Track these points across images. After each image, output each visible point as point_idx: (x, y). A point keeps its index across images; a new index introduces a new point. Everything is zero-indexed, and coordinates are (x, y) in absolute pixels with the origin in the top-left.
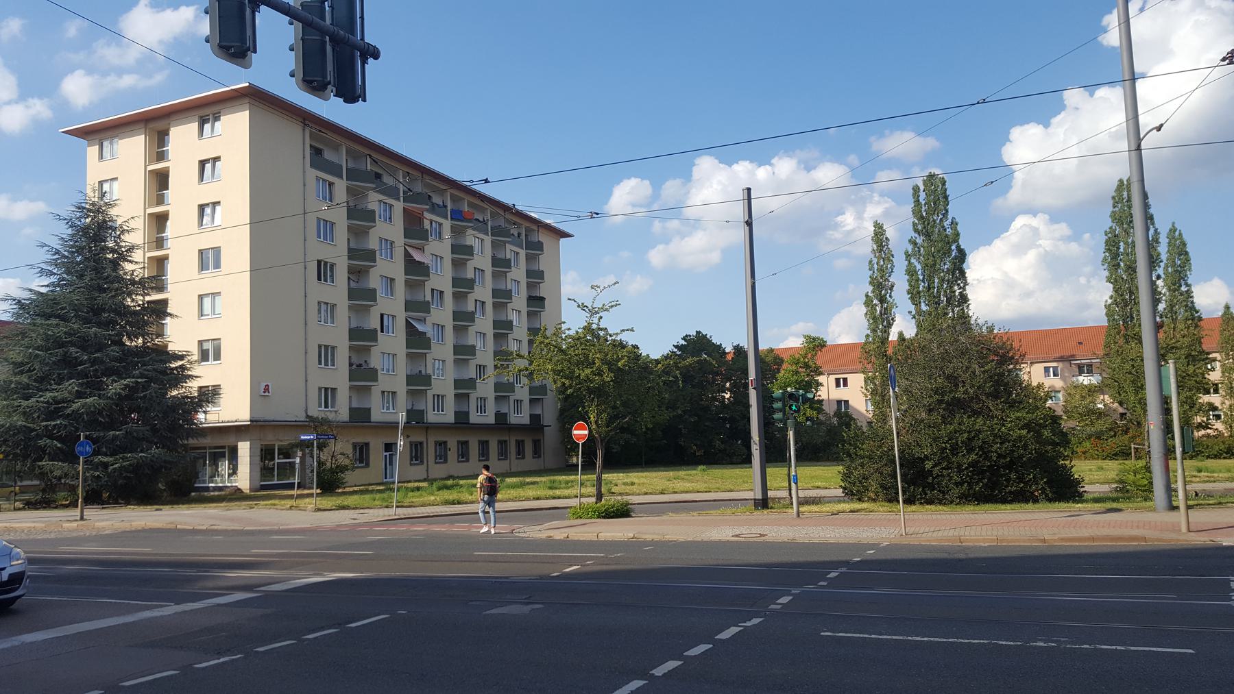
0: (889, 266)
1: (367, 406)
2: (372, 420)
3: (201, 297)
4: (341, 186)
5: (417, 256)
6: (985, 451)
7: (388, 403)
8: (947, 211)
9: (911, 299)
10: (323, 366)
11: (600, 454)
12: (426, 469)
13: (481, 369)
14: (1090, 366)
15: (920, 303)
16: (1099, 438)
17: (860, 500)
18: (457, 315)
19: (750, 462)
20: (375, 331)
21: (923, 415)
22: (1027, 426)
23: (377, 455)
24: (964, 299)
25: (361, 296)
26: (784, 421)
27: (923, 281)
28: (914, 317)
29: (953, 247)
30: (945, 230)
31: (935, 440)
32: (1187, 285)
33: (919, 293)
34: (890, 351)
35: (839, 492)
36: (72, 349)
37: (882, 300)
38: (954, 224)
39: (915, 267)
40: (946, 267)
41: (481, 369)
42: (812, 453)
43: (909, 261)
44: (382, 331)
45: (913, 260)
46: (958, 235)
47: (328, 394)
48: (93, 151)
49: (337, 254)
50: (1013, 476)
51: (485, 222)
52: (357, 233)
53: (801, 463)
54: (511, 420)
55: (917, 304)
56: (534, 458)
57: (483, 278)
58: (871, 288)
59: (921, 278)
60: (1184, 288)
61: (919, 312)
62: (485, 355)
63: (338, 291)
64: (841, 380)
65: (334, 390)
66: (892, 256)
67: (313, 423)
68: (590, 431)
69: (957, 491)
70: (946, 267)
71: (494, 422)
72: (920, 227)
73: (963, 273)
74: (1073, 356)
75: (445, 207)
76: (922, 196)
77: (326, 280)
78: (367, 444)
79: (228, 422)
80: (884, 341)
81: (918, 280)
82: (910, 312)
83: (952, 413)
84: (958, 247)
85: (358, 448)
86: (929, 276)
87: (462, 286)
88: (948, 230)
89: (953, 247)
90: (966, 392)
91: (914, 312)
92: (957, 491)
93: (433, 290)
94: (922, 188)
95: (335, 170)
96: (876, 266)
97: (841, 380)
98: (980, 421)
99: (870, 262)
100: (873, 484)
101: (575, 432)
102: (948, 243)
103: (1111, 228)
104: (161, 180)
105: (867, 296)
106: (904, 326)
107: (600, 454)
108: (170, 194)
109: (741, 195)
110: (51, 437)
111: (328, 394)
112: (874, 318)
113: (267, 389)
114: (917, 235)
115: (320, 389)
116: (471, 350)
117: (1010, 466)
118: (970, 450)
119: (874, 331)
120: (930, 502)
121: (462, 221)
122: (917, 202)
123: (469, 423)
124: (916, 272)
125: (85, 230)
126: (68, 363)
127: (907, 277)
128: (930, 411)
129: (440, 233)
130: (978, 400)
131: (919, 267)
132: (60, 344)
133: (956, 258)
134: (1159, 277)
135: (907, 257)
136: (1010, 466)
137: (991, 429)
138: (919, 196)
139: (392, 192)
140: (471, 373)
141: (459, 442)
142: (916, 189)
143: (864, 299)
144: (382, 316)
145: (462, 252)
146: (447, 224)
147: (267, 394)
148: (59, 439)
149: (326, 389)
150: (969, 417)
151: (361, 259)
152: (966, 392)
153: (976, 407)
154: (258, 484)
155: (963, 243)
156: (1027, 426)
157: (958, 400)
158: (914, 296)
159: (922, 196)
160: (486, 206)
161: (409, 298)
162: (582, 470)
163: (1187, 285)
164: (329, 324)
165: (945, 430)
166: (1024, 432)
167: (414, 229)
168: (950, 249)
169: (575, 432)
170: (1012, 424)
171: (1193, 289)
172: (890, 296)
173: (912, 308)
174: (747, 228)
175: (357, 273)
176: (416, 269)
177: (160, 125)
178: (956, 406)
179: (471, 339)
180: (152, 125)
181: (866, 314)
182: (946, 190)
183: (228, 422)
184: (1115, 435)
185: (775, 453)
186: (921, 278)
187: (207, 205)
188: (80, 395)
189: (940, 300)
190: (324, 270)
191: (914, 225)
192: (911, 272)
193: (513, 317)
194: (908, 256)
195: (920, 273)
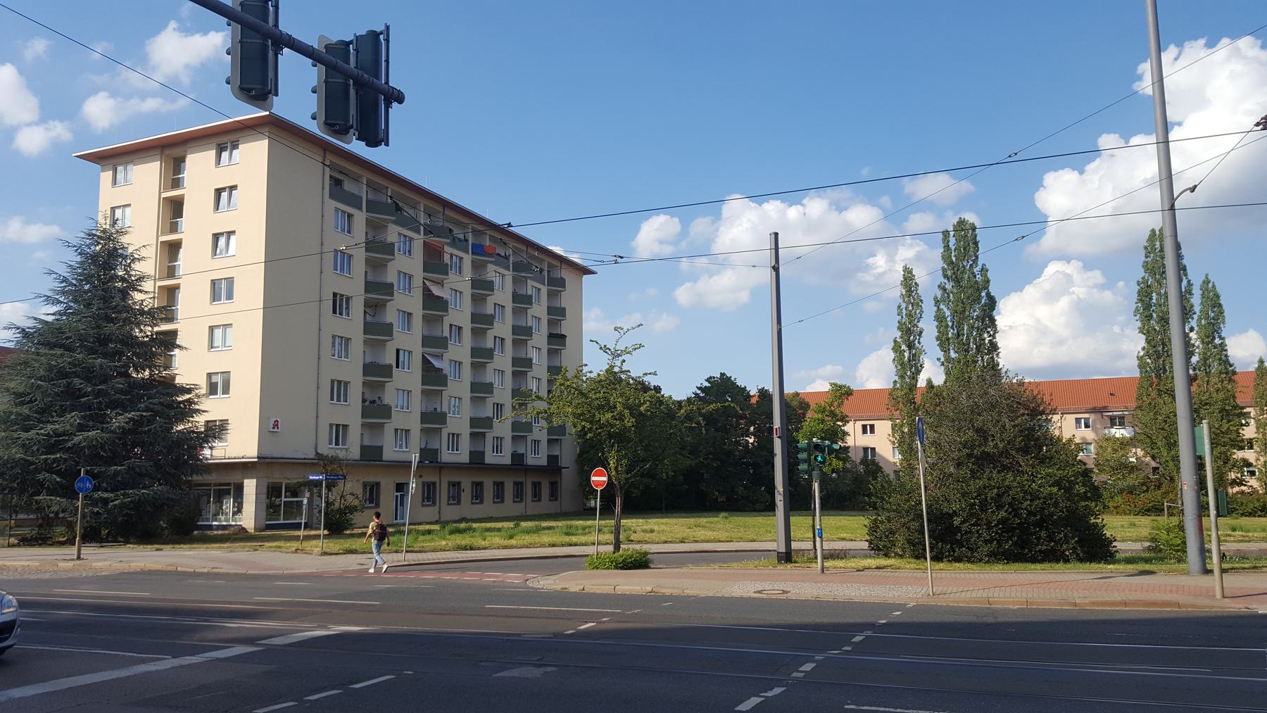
0: (918, 312)
1: (380, 445)
2: (384, 459)
3: (212, 329)
4: (360, 217)
5: (436, 291)
6: (1015, 511)
7: (401, 440)
9: (941, 345)
10: (335, 402)
11: (618, 501)
12: (438, 510)
13: (499, 407)
14: (1122, 418)
16: (1131, 493)
18: (475, 352)
19: (774, 510)
20: (391, 366)
21: (952, 469)
22: (1058, 483)
23: (388, 496)
24: (994, 347)
25: (377, 330)
28: (943, 364)
29: (983, 294)
30: (975, 276)
31: (963, 495)
32: (1221, 338)
33: (948, 339)
34: (918, 400)
36: (76, 381)
38: (984, 270)
39: (944, 313)
40: (976, 314)
41: (499, 407)
44: (397, 367)
46: (988, 281)
47: (339, 432)
48: (107, 176)
49: (354, 287)
50: (1043, 534)
51: (506, 257)
52: (376, 265)
54: (442, 457)
56: (550, 500)
57: (503, 313)
58: (900, 333)
59: (950, 324)
60: (1217, 341)
61: (948, 359)
62: (502, 392)
63: (353, 324)
64: (868, 427)
65: (345, 426)
66: (921, 301)
67: (322, 462)
70: (976, 314)
71: (468, 461)
72: (949, 273)
73: (993, 321)
74: (1105, 407)
75: (467, 241)
76: (952, 241)
77: (341, 314)
78: (378, 484)
79: (235, 458)
80: (912, 387)
81: (947, 326)
82: (939, 359)
84: (988, 294)
86: (958, 322)
87: (482, 321)
88: (978, 276)
89: (983, 294)
93: (451, 325)
95: (355, 201)
96: (904, 311)
97: (868, 427)
100: (900, 539)
101: (594, 478)
102: (978, 289)
103: (1143, 278)
104: (175, 208)
105: (895, 341)
106: (932, 372)
107: (618, 501)
108: (185, 222)
110: (50, 471)
111: (339, 432)
112: (902, 364)
113: (276, 425)
114: (946, 281)
115: (331, 425)
116: (489, 388)
117: (1040, 524)
118: (1000, 507)
119: (902, 377)
120: (958, 560)
121: (483, 255)
122: (947, 247)
123: (484, 464)
125: (94, 257)
126: (72, 395)
128: (959, 465)
129: (460, 267)
131: (948, 313)
132: (63, 374)
133: (985, 305)
134: (1192, 329)
135: (936, 303)
136: (1040, 524)
138: (948, 241)
139: (412, 225)
140: (488, 411)
141: (473, 483)
144: (398, 351)
145: (482, 287)
146: (468, 259)
147: (276, 430)
148: (58, 473)
149: (338, 426)
151: (378, 291)
154: (264, 523)
155: (993, 290)
156: (1058, 483)
158: (943, 342)
159: (952, 241)
160: (544, 258)
161: (426, 333)
162: (823, 507)
163: (1221, 338)
164: (343, 359)
165: (974, 485)
166: (1055, 489)
167: (434, 262)
169: (594, 478)
170: (1043, 481)
171: (1227, 341)
172: (919, 343)
173: (941, 355)
174: (774, 273)
175: (373, 307)
176: (433, 303)
177: (176, 152)
178: (985, 460)
179: (489, 376)
180: (167, 152)
181: (894, 360)
183: (235, 458)
185: (799, 501)
186: (950, 324)
187: (222, 234)
188: (81, 428)
189: (969, 347)
190: (339, 304)
191: (944, 270)
192: (940, 318)
193: (533, 355)
194: (937, 302)
195: (949, 319)
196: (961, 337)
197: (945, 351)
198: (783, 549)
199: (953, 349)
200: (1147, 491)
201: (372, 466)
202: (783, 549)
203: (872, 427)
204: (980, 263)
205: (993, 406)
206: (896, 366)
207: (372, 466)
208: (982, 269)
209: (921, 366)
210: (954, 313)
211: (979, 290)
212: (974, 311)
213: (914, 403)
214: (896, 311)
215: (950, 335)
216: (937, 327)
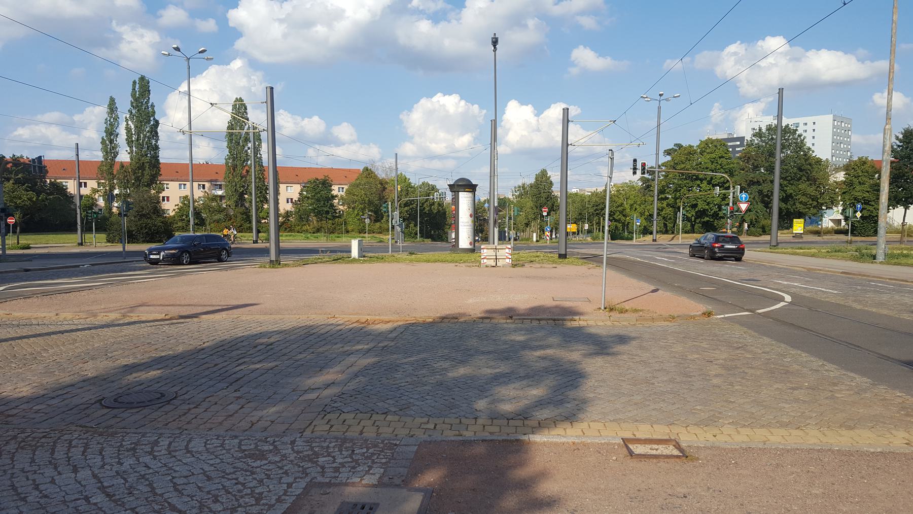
6: (150, 229)
8: (149, 98)
9: (128, 143)
11: (18, 228)
14: (220, 185)
15: (132, 146)
16: (218, 222)
17: (112, 243)
21: (133, 218)
22: (162, 222)
24: (156, 148)
26: (92, 219)
27: (134, 134)
28: (129, 153)
29: (152, 119)
30: (148, 108)
33: (132, 141)
35: (106, 241)
37: (111, 141)
38: (153, 106)
39: (131, 126)
40: (147, 129)
42: (99, 229)
43: (127, 123)
45: (130, 123)
46: (154, 112)
50: (158, 236)
53: (99, 231)
55: (131, 147)
58: (105, 134)
59: (134, 133)
60: (259, 156)
61: (132, 152)
64: (83, 183)
66: (119, 118)
68: (16, 220)
69: (141, 240)
70: (147, 129)
72: (134, 104)
73: (157, 133)
74: (217, 180)
76: (137, 86)
81: (132, 134)
82: (127, 151)
83: (142, 218)
84: (154, 119)
85: (507, 239)
86: (138, 133)
88: (150, 109)
89: (152, 119)
90: (146, 212)
91: (129, 151)
92: (141, 240)
94: (138, 82)
96: (109, 122)
97: (83, 183)
98: (149, 220)
99: (106, 119)
100: (117, 238)
101: (8, 220)
102: (149, 116)
103: (231, 120)
105: (103, 139)
106: (124, 156)
109: (75, 146)
112: (107, 152)
114: (132, 108)
118: (146, 229)
120: (134, 243)
122: (134, 89)
124: (131, 129)
127: (126, 131)
128: (135, 217)
130: (149, 215)
131: (133, 127)
133: (153, 125)
134: (249, 148)
135: (126, 120)
136: (157, 233)
137: (152, 223)
142: (134, 82)
143: (101, 140)
150: (146, 219)
152: (146, 212)
153: (149, 216)
155: (157, 117)
156: (162, 222)
157: (144, 214)
158: (129, 142)
163: (260, 154)
165: (139, 223)
168: (150, 120)
170: (158, 221)
171: (263, 156)
172: (116, 141)
173: (128, 149)
174: (77, 156)
181: (102, 149)
182: (149, 86)
184: (225, 222)
185: (87, 229)
186: (134, 133)
189: (143, 146)
191: (132, 103)
192: (128, 129)
194: (127, 120)
195: (133, 130)
196: (139, 141)
197: (130, 147)
198: (80, 242)
199: (135, 147)
200: (225, 222)
201: (877, 277)
202: (80, 242)
203: (85, 184)
204: (151, 101)
205: (145, 200)
206: (103, 153)
207: (877, 277)
208: (152, 106)
209: (117, 153)
210: (136, 127)
211: (149, 117)
212: (147, 127)
213: (113, 174)
214: (104, 121)
215: (133, 139)
216: (126, 133)
